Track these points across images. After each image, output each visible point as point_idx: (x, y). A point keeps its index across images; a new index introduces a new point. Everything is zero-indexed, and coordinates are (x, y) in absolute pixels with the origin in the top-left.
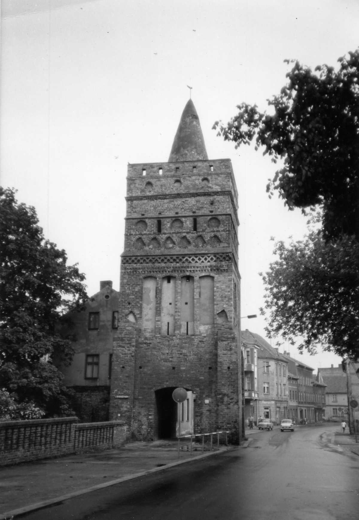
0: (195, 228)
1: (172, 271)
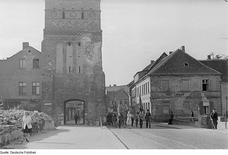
0: (83, 18)
1: (71, 40)
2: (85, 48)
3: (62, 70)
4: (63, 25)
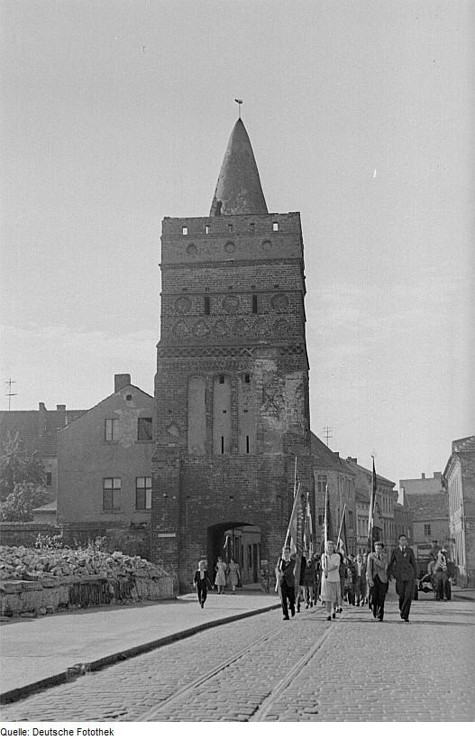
2: (261, 387)
3: (202, 447)
4: (206, 330)
